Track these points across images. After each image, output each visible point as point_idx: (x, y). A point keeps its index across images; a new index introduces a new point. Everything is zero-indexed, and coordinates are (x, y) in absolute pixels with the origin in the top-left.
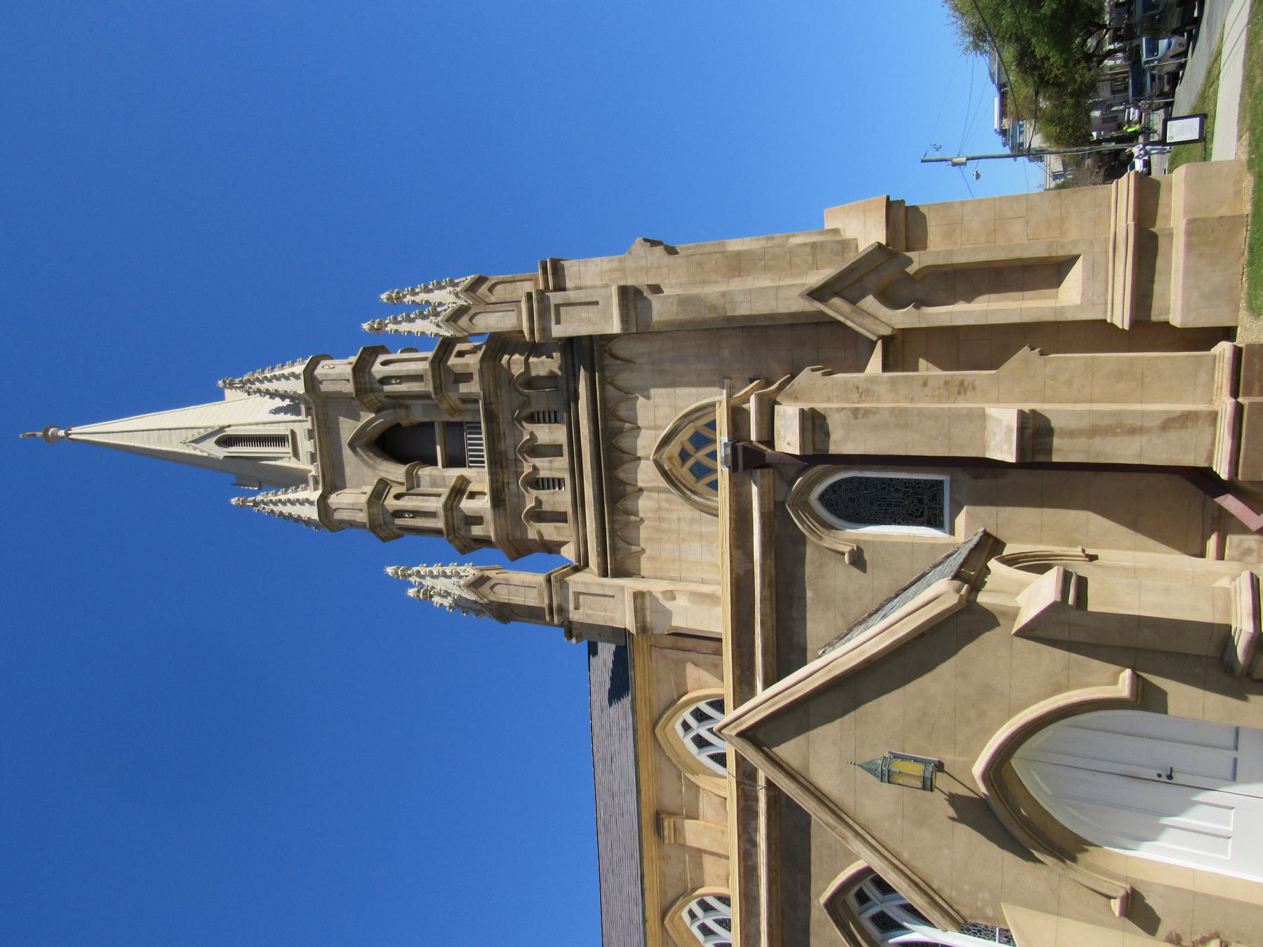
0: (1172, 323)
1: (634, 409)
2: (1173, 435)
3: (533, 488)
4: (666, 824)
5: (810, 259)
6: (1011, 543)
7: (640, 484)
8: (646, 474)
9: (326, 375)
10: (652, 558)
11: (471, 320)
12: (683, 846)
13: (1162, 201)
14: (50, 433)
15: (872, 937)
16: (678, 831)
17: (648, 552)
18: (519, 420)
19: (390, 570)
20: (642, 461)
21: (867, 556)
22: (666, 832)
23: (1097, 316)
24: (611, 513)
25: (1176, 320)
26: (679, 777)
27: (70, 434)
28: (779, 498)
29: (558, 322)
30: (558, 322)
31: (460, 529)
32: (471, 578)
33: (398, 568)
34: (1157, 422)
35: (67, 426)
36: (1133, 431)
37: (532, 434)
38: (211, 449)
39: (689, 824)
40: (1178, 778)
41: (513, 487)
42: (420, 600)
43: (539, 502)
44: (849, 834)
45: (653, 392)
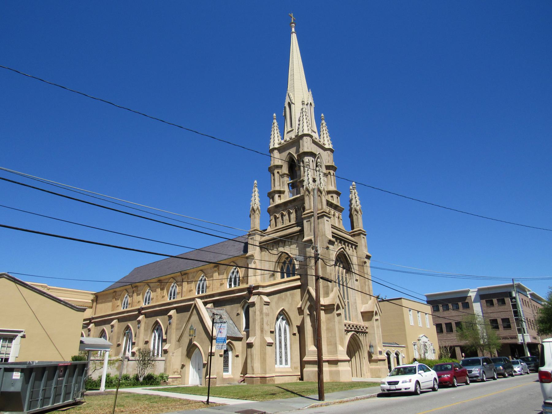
0: (304, 369)
1: (294, 244)
2: (251, 368)
3: (281, 215)
4: (216, 268)
5: (325, 285)
6: (242, 343)
7: (279, 249)
8: (281, 249)
9: (304, 141)
10: (265, 254)
11: (307, 195)
12: (213, 273)
13: (334, 365)
14: (292, 25)
15: (266, 296)
16: (215, 271)
17: (266, 253)
18: (295, 208)
19: (256, 182)
20: (283, 248)
21: (239, 316)
22: (214, 269)
23: (307, 354)
24: (272, 242)
25: (305, 370)
26: (225, 270)
27: (292, 33)
28: (246, 298)
29: (307, 221)
30: (307, 221)
31: (271, 196)
32: (254, 207)
33: (256, 184)
34: (252, 365)
35: (297, 32)
36: (251, 361)
37: (292, 213)
38: (287, 100)
39: (217, 274)
40: (199, 370)
41: (281, 210)
42: (321, 118)
43: (278, 218)
44: (186, 323)
45: (298, 248)
